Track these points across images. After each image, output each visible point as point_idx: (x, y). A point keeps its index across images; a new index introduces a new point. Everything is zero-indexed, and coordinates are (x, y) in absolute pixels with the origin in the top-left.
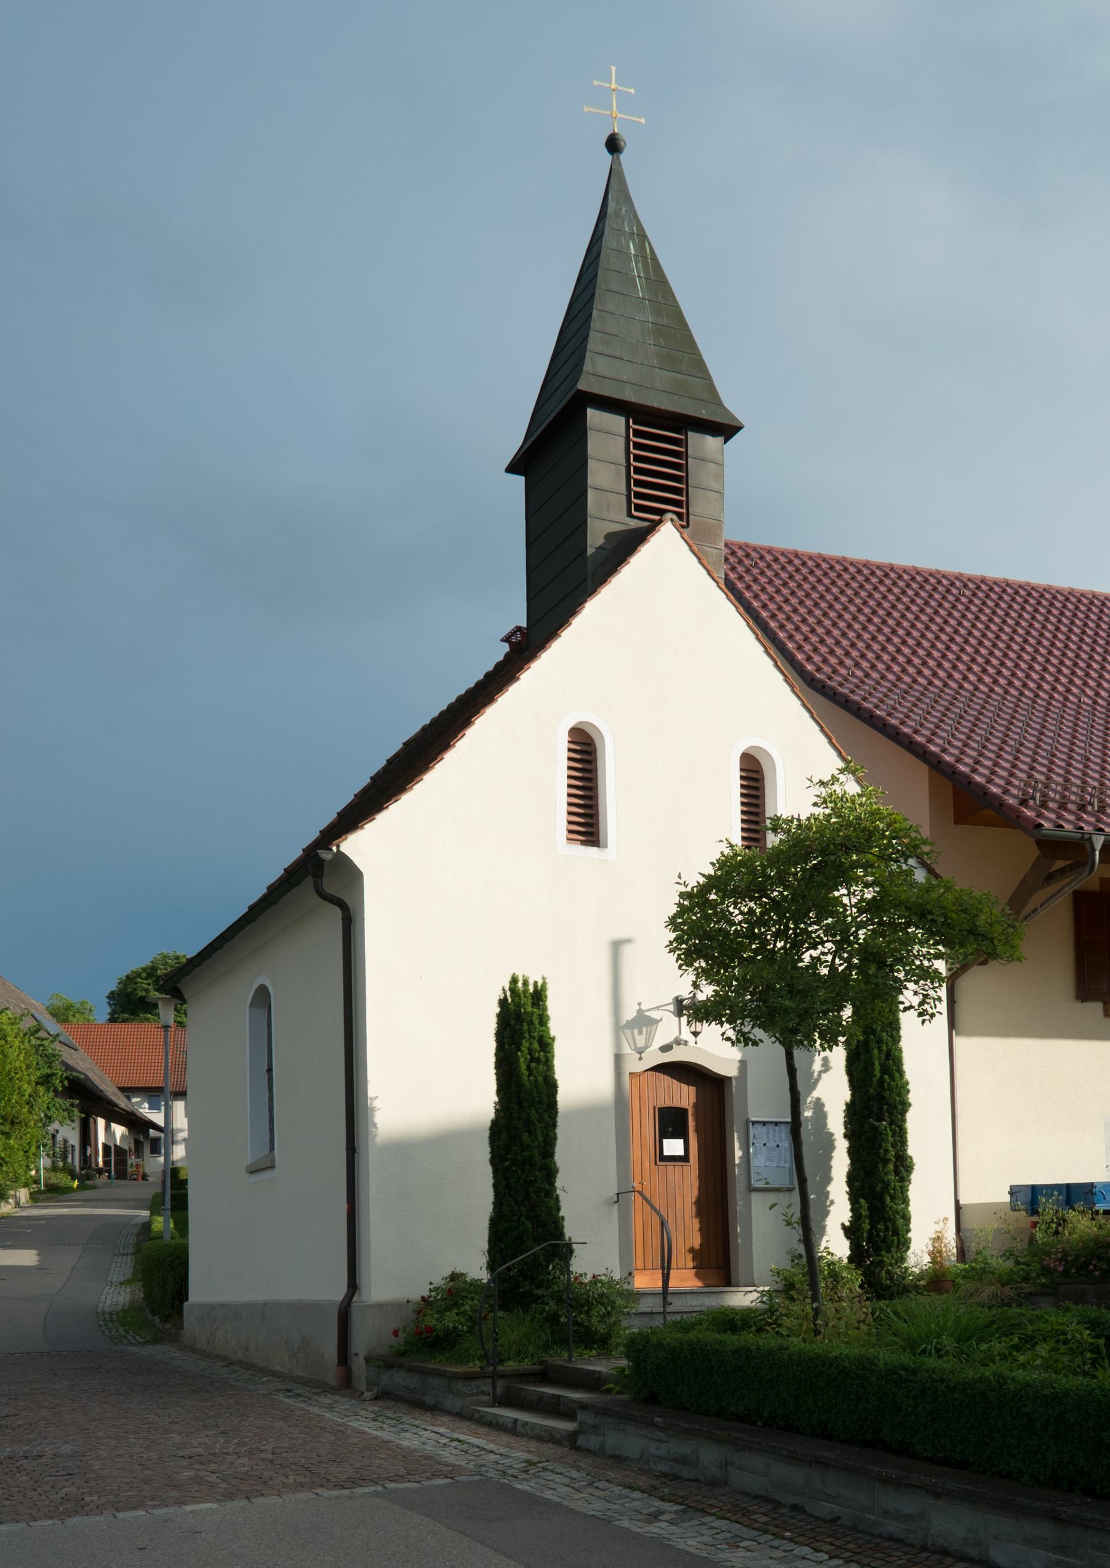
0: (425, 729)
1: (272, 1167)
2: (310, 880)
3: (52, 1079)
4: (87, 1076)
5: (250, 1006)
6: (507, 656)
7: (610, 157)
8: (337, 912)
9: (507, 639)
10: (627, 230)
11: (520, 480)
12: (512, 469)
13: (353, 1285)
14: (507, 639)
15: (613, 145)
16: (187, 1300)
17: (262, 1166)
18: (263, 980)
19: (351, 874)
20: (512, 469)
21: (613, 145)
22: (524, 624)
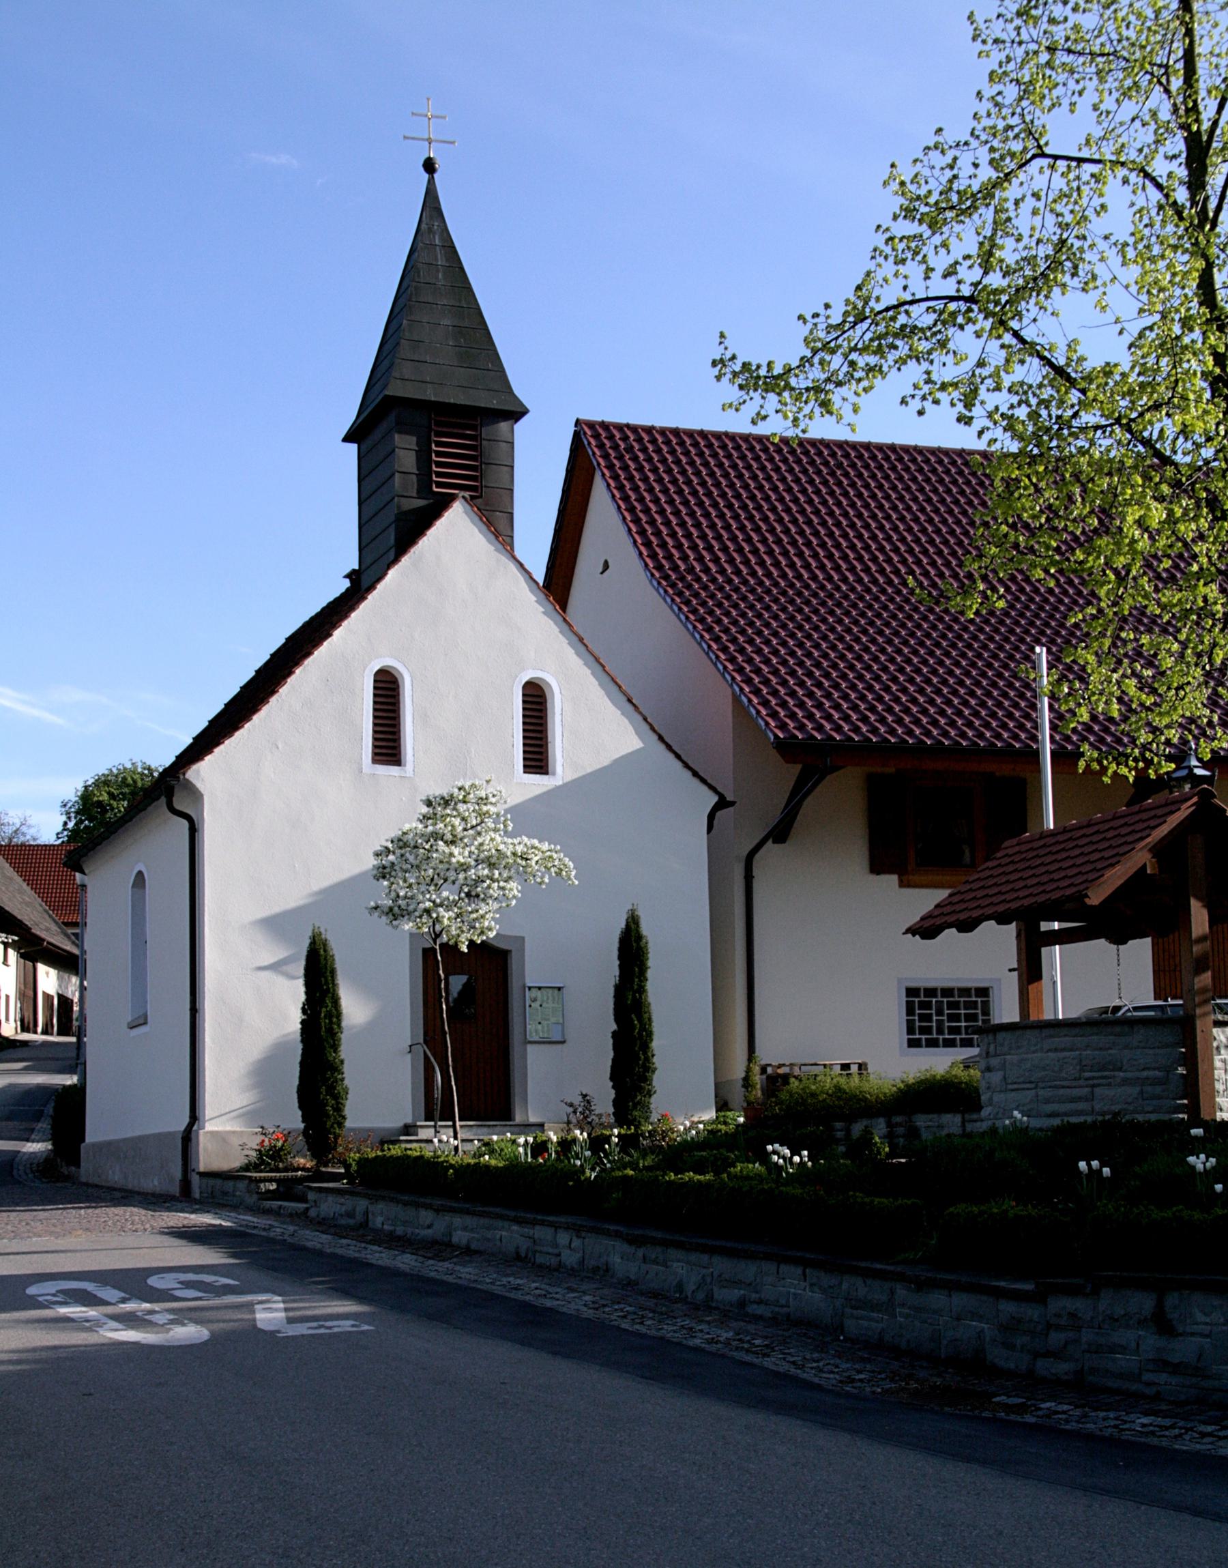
0: (323, 609)
1: (145, 1023)
2: (163, 800)
3: (24, 834)
4: (883, 751)
5: (133, 886)
6: (348, 590)
7: (426, 176)
8: (185, 824)
9: (348, 576)
10: (437, 242)
11: (353, 447)
12: (347, 439)
13: (195, 1116)
14: (348, 576)
15: (429, 166)
16: (83, 1140)
17: (140, 1021)
18: (140, 867)
19: (195, 795)
20: (347, 439)
21: (429, 166)
22: (357, 567)
